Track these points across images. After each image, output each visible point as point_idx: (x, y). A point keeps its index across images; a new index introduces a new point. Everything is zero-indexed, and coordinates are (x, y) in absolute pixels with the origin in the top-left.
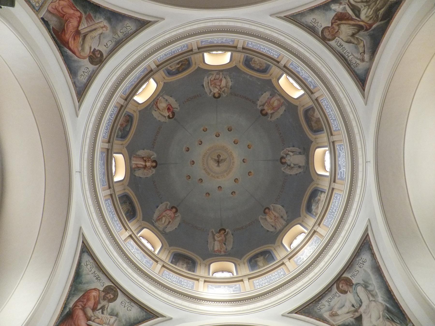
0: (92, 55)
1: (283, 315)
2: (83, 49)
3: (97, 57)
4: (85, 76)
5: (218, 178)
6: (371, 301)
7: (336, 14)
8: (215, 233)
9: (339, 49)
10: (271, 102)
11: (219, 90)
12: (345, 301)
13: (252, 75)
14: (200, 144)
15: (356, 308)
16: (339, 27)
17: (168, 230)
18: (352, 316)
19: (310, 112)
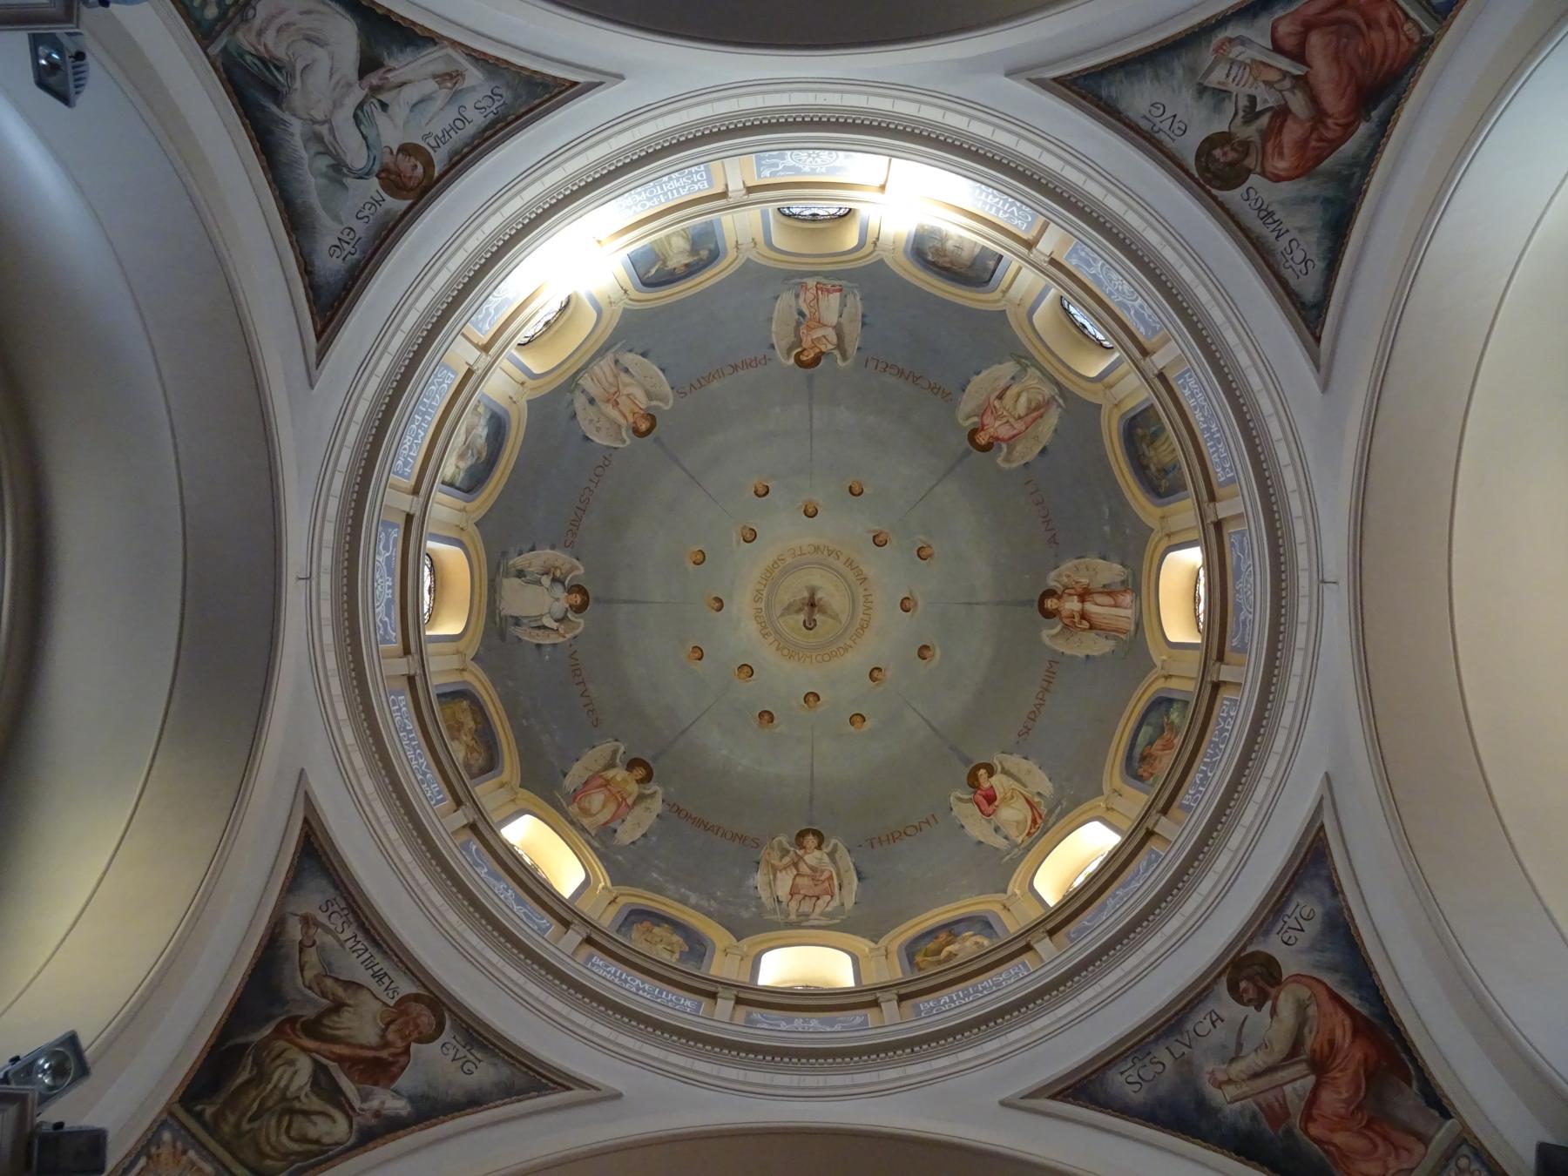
0: (1269, 989)
1: (621, 77)
2: (1301, 1008)
3: (1250, 979)
4: (1297, 914)
5: (817, 549)
6: (327, 121)
7: (394, 1078)
8: (836, 352)
9: (383, 964)
10: (612, 807)
11: (801, 858)
12: (406, 123)
13: (680, 906)
14: (879, 669)
15: (376, 99)
16: (383, 1037)
17: (1008, 368)
18: (389, 75)
19: (479, 760)
